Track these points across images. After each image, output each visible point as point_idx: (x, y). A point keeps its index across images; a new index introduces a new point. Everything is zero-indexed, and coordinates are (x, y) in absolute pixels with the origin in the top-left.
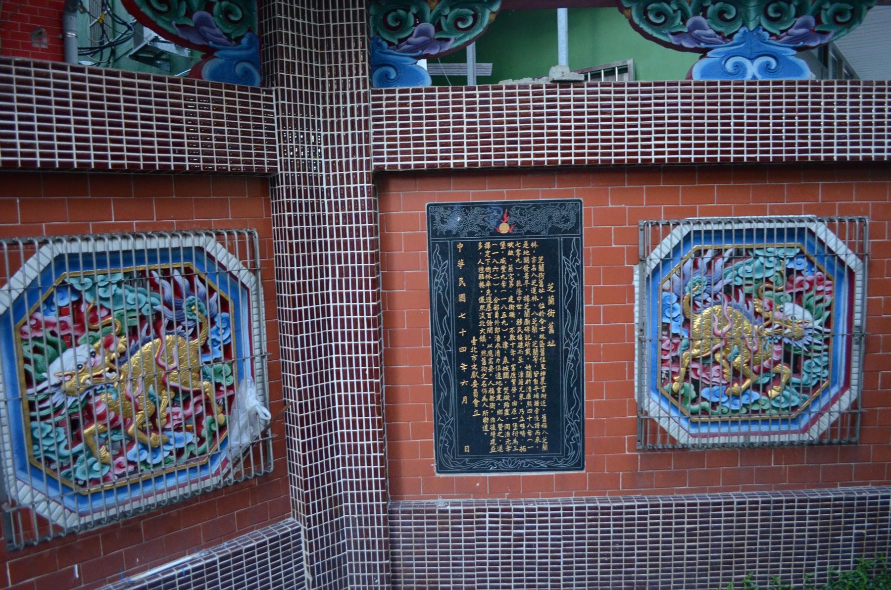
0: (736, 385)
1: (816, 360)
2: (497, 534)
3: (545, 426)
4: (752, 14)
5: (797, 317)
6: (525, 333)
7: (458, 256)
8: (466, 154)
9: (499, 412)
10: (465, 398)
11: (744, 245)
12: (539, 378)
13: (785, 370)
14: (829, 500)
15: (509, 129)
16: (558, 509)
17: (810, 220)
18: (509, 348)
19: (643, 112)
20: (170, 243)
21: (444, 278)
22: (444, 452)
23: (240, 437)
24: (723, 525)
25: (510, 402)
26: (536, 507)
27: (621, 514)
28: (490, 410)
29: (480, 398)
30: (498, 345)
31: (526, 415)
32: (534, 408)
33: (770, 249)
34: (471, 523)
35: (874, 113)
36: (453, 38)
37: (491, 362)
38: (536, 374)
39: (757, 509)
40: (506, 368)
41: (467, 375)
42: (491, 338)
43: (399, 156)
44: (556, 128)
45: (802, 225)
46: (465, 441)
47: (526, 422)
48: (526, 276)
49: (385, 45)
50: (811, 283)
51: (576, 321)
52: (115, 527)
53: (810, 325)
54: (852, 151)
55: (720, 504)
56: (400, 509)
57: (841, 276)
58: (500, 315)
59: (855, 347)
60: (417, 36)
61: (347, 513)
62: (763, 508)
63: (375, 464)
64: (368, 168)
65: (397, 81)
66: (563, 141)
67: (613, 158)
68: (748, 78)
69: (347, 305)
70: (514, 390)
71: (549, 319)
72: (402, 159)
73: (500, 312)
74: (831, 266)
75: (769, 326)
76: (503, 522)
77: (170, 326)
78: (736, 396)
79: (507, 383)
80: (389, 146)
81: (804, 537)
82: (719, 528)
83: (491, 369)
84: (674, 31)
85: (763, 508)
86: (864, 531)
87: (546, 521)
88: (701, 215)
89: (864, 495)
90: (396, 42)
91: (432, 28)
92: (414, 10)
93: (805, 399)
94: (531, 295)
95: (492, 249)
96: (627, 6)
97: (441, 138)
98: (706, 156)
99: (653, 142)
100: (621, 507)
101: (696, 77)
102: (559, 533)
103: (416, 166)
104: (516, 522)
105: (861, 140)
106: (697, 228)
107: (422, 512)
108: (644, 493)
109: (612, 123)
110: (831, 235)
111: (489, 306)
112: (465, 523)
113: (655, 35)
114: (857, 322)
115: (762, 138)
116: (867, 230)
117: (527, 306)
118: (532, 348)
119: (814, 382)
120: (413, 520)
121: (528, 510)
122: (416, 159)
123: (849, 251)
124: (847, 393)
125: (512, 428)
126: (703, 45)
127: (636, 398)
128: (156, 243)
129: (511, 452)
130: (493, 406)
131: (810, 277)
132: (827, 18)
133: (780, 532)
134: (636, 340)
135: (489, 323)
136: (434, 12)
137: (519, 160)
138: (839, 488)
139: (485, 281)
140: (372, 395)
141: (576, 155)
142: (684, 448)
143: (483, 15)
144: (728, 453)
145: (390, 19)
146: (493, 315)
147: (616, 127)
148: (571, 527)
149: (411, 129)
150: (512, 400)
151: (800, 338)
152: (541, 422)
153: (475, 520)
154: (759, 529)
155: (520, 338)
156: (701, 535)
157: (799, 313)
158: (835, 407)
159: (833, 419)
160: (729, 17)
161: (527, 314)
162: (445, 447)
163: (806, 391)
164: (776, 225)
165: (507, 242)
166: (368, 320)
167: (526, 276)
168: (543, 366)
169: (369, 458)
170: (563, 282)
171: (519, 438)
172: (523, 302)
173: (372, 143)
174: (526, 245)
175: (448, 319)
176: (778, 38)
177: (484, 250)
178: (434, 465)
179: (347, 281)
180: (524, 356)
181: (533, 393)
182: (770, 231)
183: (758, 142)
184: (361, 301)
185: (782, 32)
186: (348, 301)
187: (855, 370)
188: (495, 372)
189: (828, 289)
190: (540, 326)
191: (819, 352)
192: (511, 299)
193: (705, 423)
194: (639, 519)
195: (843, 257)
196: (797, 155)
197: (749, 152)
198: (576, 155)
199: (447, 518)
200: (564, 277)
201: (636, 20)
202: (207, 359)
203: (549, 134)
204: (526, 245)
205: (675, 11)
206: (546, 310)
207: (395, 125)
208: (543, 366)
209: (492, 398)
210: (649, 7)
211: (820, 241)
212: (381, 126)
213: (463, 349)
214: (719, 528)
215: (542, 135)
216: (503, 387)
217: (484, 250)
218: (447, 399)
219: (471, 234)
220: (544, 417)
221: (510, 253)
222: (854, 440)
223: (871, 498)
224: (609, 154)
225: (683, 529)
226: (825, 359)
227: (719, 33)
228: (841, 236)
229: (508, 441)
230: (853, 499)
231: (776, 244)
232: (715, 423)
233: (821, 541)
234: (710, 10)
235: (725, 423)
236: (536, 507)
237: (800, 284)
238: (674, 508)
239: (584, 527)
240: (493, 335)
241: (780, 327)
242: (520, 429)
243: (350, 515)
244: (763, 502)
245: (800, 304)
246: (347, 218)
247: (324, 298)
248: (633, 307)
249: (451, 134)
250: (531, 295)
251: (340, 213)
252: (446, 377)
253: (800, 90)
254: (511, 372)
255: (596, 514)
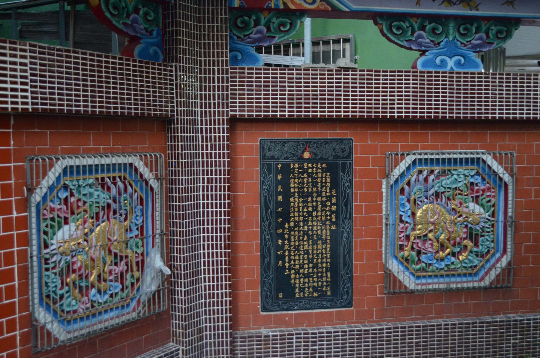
0: (441, 253)
1: (487, 237)
2: (300, 350)
3: (329, 279)
4: (451, 31)
5: (476, 211)
6: (318, 220)
7: (278, 172)
8: (287, 109)
9: (301, 271)
10: (280, 263)
11: (447, 167)
12: (326, 249)
13: (468, 243)
14: (496, 322)
15: (313, 95)
16: (338, 332)
17: (483, 153)
18: (303, 231)
19: (390, 88)
20: (94, 162)
21: (269, 186)
22: (266, 297)
23: (150, 285)
24: (436, 339)
25: (308, 265)
26: (325, 331)
27: (376, 334)
28: (295, 269)
29: (289, 262)
30: (301, 229)
31: (318, 273)
32: (322, 268)
33: (460, 170)
34: (284, 343)
35: (497, 80)
36: (277, 36)
37: (297, 239)
38: (324, 246)
39: (455, 328)
40: (306, 243)
41: (282, 248)
42: (297, 224)
43: (246, 109)
44: (340, 95)
45: (478, 156)
46: (279, 291)
47: (318, 277)
48: (319, 185)
49: (235, 38)
50: (484, 191)
51: (348, 213)
52: (84, 341)
53: (483, 216)
54: (507, 114)
55: (434, 326)
56: (239, 336)
57: (500, 187)
58: (303, 209)
59: (509, 229)
60: (255, 34)
61: (206, 339)
62: (459, 328)
63: (226, 305)
64: (227, 116)
65: (242, 61)
66: (344, 103)
67: (373, 114)
68: (448, 69)
69: (210, 202)
70: (311, 257)
71: (332, 212)
72: (248, 111)
73: (303, 207)
74: (495, 181)
75: (460, 216)
76: (304, 342)
77: (115, 212)
78: (442, 260)
79: (307, 252)
80: (240, 103)
81: (483, 345)
82: (434, 341)
83: (297, 243)
84: (407, 39)
85: (459, 328)
86: (517, 341)
87: (331, 340)
88: (422, 149)
89: (516, 318)
90: (242, 37)
91: (265, 30)
92: (254, 17)
93: (481, 261)
94: (322, 197)
95: (299, 168)
96: (380, 22)
97: (273, 99)
98: (426, 115)
99: (396, 106)
100: (375, 330)
101: (420, 68)
102: (338, 348)
103: (256, 115)
104: (312, 342)
105: (511, 108)
106: (419, 157)
107: (253, 337)
108: (388, 321)
109: (373, 94)
110: (494, 162)
111: (296, 203)
112: (281, 344)
113: (396, 41)
114: (510, 214)
115: (457, 105)
116: (515, 160)
117: (319, 203)
118: (322, 230)
119: (486, 251)
120: (247, 343)
121: (320, 333)
122: (256, 111)
123: (505, 172)
124: (505, 257)
125: (309, 281)
126: (423, 48)
127: (384, 261)
128: (106, 161)
129: (308, 297)
130: (297, 267)
131: (482, 187)
132: (493, 35)
133: (469, 343)
134: (384, 225)
135: (296, 214)
136: (266, 19)
137: (319, 114)
138: (502, 315)
139: (294, 188)
140: (225, 260)
141: (352, 112)
142: (412, 292)
143: (296, 24)
144: (437, 294)
145: (238, 22)
146: (299, 209)
147: (375, 96)
148: (346, 343)
149: (254, 92)
150: (309, 263)
151: (478, 224)
152: (327, 277)
153: (287, 341)
154: (457, 341)
155: (315, 223)
156: (423, 346)
157: (478, 209)
158: (498, 265)
159: (497, 273)
160: (438, 32)
161: (319, 209)
162: (267, 295)
163: (482, 256)
164: (463, 156)
165: (308, 164)
166: (225, 212)
167: (319, 185)
168: (328, 241)
169: (222, 302)
170: (341, 189)
171: (314, 287)
172: (317, 201)
173: (230, 100)
174: (319, 165)
175: (271, 212)
176: (465, 46)
177: (294, 168)
178: (260, 307)
179: (212, 187)
180: (317, 235)
181: (322, 258)
182: (461, 159)
183: (455, 107)
184: (220, 199)
185: (467, 42)
186: (212, 199)
187: (509, 243)
188: (299, 245)
189: (493, 194)
190: (327, 216)
191: (488, 232)
192: (310, 199)
193: (424, 277)
194: (387, 337)
195: (501, 175)
196: (476, 115)
197: (450, 113)
198: (352, 112)
199: (269, 340)
200: (341, 186)
201: (385, 31)
202: (131, 236)
203: (336, 99)
204: (319, 165)
205: (407, 27)
206: (330, 206)
207: (244, 90)
208: (328, 241)
209: (297, 262)
210: (393, 24)
211: (489, 166)
212: (236, 90)
213: (280, 231)
214: (434, 341)
215: (332, 99)
216: (304, 255)
217: (294, 168)
218: (269, 263)
219: (286, 158)
220: (329, 274)
221: (310, 171)
222: (509, 285)
223: (521, 320)
224: (371, 112)
225: (412, 343)
226: (492, 236)
227: (432, 41)
228: (500, 163)
229: (307, 289)
230: (510, 321)
231: (464, 167)
232: (430, 276)
233: (493, 348)
234: (427, 28)
235: (436, 276)
236: (325, 331)
237: (478, 191)
238: (407, 329)
239: (353, 343)
240: (299, 222)
241: (466, 217)
242: (314, 282)
243: (208, 340)
244: (459, 324)
245: (477, 203)
246: (213, 147)
247: (198, 198)
248: (382, 205)
249: (279, 96)
250: (322, 197)
251: (209, 144)
252: (269, 249)
253: (478, 77)
254: (309, 245)
255: (361, 335)
